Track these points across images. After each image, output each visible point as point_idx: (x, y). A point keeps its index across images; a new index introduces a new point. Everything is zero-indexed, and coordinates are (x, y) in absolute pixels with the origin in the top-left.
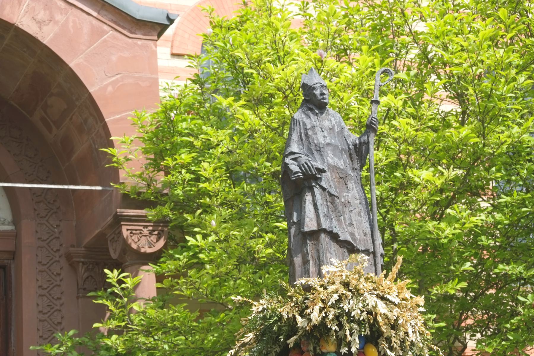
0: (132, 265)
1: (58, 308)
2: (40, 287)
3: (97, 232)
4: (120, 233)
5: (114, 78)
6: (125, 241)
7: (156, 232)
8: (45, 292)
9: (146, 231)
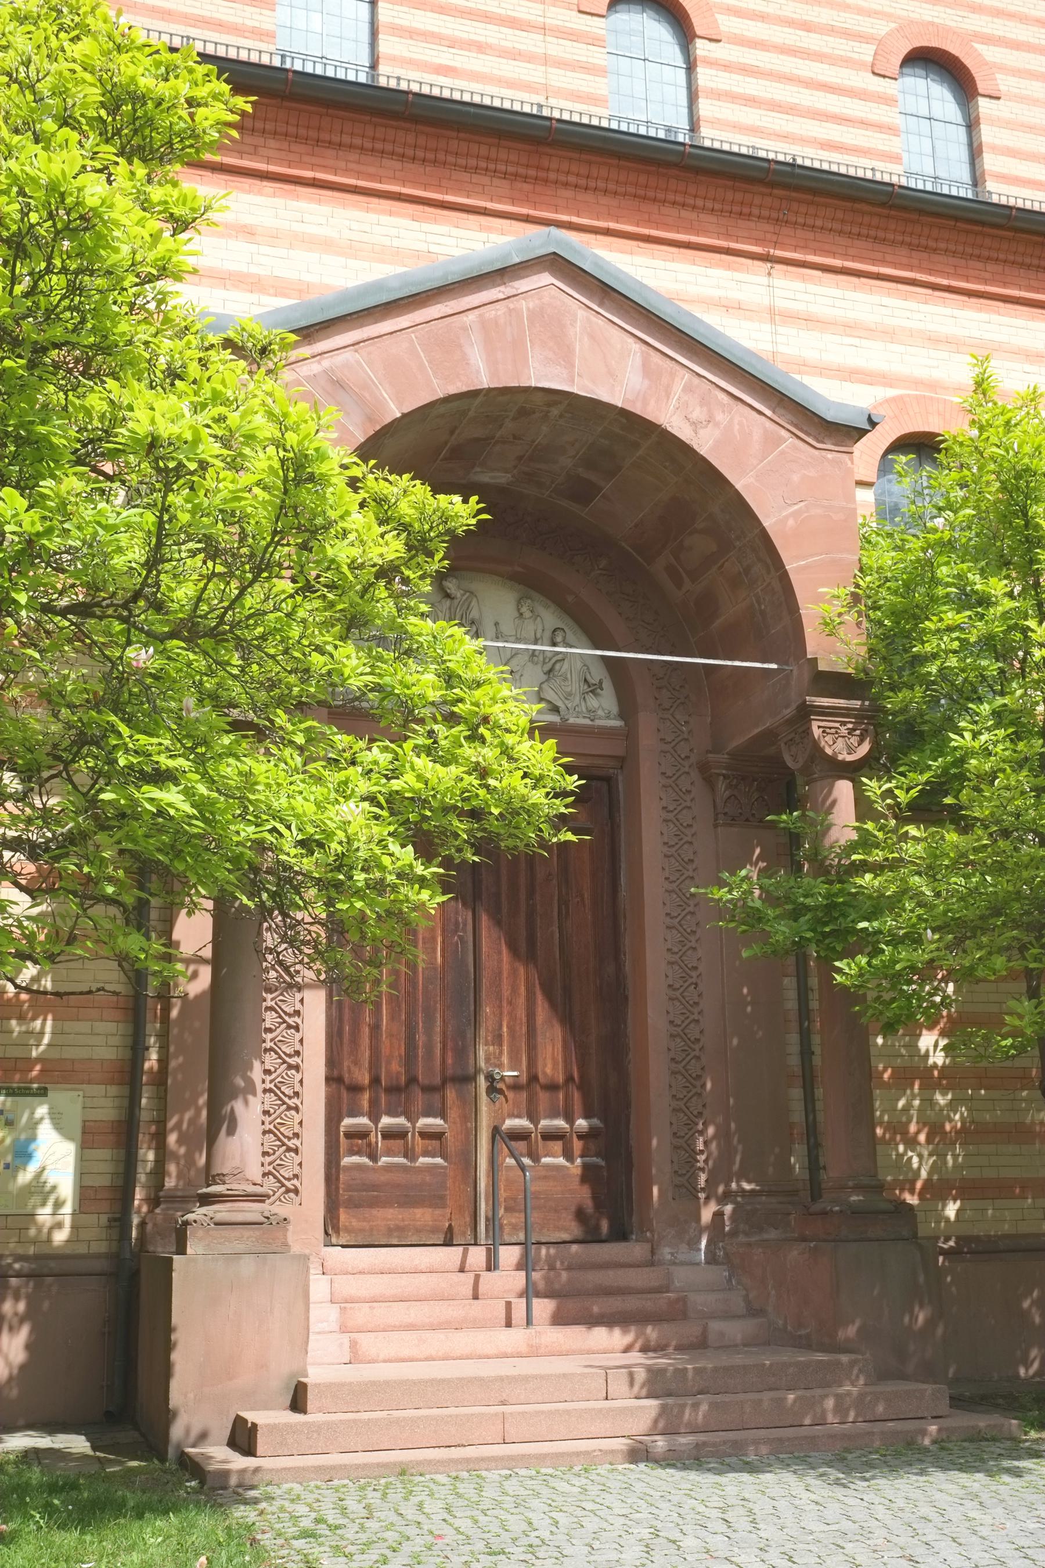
0: (822, 778)
1: (689, 839)
2: (664, 808)
3: (756, 731)
4: (808, 731)
5: (796, 507)
6: (816, 744)
7: (858, 732)
8: (671, 816)
9: (843, 730)
